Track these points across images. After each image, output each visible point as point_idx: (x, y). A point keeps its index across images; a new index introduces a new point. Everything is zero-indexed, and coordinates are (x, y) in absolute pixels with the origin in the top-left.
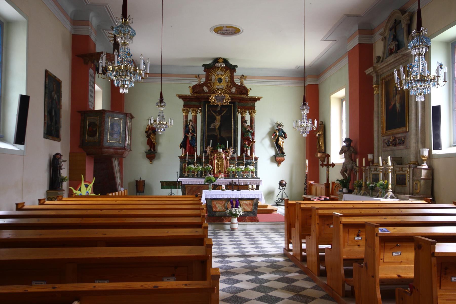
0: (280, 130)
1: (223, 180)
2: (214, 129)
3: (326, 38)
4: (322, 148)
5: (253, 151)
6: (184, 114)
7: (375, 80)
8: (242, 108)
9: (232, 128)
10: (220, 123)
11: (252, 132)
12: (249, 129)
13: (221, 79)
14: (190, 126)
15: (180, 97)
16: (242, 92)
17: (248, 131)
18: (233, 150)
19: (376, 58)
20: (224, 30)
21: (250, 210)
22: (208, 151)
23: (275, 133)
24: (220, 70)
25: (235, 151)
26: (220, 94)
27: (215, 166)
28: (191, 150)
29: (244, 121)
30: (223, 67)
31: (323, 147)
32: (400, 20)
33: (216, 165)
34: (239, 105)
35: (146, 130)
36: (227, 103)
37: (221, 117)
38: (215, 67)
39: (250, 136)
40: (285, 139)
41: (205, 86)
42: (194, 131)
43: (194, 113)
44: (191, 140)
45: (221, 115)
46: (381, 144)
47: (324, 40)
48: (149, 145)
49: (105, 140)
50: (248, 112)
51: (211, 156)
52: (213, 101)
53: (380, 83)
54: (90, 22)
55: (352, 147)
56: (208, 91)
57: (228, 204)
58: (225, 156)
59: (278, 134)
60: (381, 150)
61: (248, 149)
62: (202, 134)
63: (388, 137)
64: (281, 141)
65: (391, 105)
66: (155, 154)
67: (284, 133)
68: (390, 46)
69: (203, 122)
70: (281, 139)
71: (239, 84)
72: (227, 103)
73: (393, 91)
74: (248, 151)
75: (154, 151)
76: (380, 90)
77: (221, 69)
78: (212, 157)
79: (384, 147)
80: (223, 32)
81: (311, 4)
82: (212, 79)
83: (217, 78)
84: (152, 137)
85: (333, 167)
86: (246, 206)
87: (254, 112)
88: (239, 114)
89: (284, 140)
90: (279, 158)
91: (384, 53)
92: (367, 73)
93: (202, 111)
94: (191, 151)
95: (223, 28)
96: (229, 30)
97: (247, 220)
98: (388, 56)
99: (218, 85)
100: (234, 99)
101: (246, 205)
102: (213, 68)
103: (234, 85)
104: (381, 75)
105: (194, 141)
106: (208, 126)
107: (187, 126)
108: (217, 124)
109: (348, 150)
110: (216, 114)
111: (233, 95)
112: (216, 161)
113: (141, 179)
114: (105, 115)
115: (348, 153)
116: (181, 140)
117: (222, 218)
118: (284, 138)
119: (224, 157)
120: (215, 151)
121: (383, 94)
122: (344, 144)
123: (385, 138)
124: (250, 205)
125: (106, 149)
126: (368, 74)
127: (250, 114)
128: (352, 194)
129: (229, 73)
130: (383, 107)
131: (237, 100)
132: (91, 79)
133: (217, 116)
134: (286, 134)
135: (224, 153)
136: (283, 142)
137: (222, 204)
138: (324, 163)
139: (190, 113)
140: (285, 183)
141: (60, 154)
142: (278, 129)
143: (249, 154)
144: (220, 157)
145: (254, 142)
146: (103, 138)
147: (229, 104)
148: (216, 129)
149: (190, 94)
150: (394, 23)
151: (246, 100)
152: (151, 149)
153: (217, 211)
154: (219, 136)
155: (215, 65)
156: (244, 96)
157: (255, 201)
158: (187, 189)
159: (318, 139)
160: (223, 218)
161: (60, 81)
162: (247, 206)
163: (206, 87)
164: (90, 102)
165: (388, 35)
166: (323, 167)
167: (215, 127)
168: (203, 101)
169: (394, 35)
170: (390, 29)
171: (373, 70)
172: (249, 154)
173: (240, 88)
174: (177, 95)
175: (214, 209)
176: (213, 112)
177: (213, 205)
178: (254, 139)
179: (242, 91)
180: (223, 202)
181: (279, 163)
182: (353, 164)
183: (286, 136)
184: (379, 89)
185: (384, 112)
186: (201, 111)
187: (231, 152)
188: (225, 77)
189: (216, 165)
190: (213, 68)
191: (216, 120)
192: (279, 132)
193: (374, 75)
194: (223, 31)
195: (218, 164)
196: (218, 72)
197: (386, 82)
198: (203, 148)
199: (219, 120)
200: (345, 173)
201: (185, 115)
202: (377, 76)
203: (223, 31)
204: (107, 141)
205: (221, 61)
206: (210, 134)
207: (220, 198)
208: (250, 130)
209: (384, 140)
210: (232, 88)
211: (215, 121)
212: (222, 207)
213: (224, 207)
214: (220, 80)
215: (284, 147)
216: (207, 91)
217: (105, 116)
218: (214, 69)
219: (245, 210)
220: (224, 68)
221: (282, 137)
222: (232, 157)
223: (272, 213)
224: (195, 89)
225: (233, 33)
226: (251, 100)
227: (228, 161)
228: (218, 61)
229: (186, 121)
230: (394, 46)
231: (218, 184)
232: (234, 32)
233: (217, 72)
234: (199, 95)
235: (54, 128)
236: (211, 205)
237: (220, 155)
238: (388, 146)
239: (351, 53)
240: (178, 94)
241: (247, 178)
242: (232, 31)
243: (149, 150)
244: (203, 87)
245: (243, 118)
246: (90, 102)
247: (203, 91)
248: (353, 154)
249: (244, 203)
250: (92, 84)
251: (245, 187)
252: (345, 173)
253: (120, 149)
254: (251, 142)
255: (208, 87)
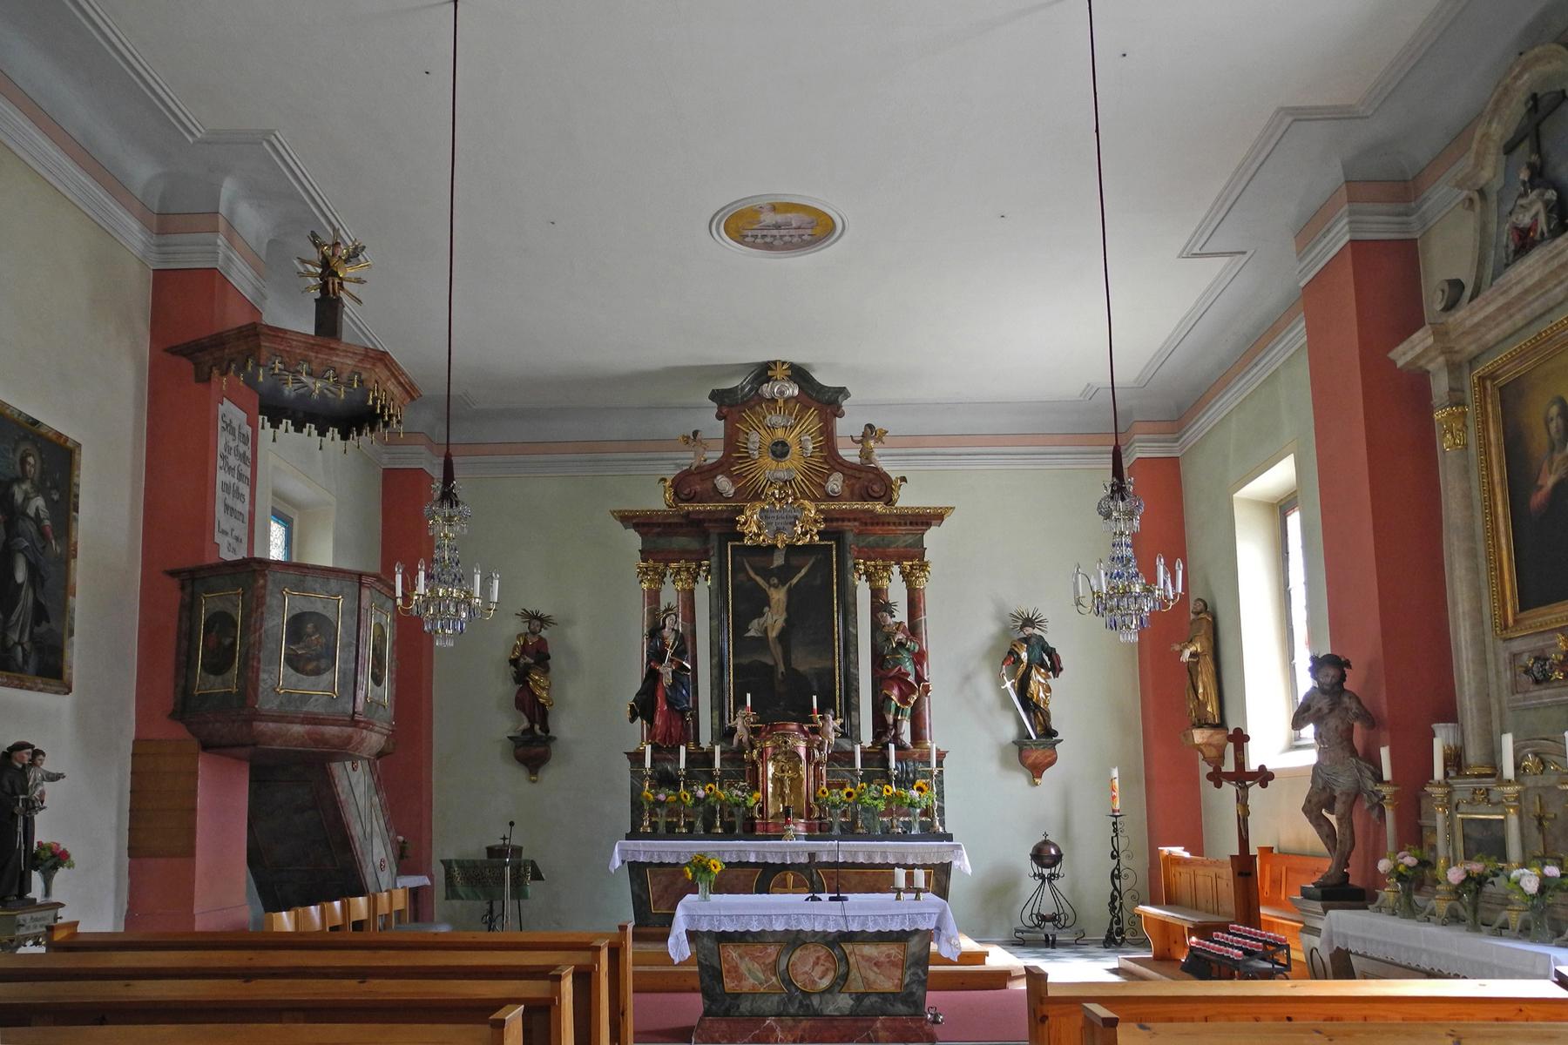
0: (1033, 640)
1: (801, 845)
2: (762, 642)
3: (1199, 245)
4: (1209, 709)
5: (925, 724)
6: (645, 586)
7: (1440, 385)
8: (873, 555)
9: (836, 636)
10: (784, 616)
11: (917, 648)
12: (900, 636)
13: (784, 444)
14: (666, 630)
15: (629, 519)
16: (870, 490)
17: (901, 644)
18: (839, 721)
19: (1443, 291)
20: (768, 227)
21: (893, 989)
22: (738, 727)
23: (1013, 654)
24: (780, 408)
25: (849, 732)
26: (780, 500)
27: (770, 790)
28: (674, 723)
29: (880, 605)
30: (792, 397)
31: (1214, 704)
32: (1558, 88)
33: (770, 785)
34: (861, 544)
35: (513, 653)
36: (808, 536)
37: (790, 592)
38: (762, 399)
39: (909, 667)
40: (1056, 675)
41: (721, 473)
42: (685, 646)
43: (681, 580)
44: (673, 687)
45: (787, 585)
46: (1498, 673)
47: (1195, 255)
48: (523, 710)
49: (262, 686)
50: (896, 569)
51: (753, 747)
52: (755, 529)
53: (1470, 396)
54: (221, 219)
55: (1353, 696)
56: (735, 493)
57: (793, 958)
58: (808, 750)
59: (1024, 656)
60: (1500, 702)
61: (902, 720)
62: (715, 660)
63: (1537, 643)
64: (1039, 682)
65: (1541, 487)
66: (549, 746)
67: (1051, 653)
68: (1513, 219)
69: (716, 614)
70: (1039, 678)
71: (857, 460)
72: (808, 536)
73: (1547, 422)
74: (901, 726)
75: (544, 734)
76: (1472, 429)
77: (782, 405)
78: (755, 752)
79: (1515, 688)
80: (764, 236)
81: (1124, 55)
82: (750, 446)
83: (768, 441)
84: (535, 681)
85: (1264, 785)
86: (875, 969)
87: (923, 566)
88: (860, 579)
89: (1052, 682)
90: (1036, 755)
91: (1481, 262)
92: (1400, 364)
93: (713, 571)
94: (673, 730)
95: (762, 217)
96: (788, 225)
97: (881, 1034)
98: (1507, 265)
99: (771, 469)
100: (837, 520)
101: (875, 964)
102: (752, 403)
103: (837, 467)
104: (1470, 362)
105: (684, 692)
106: (740, 627)
107: (655, 632)
108: (774, 619)
109: (1331, 710)
110: (768, 583)
111: (834, 506)
112: (771, 769)
113: (507, 842)
114: (266, 581)
115: (1333, 722)
116: (636, 685)
117: (768, 1022)
118: (1050, 674)
119: (802, 753)
120: (766, 727)
121: (1490, 444)
122: (1343, 659)
123: (1516, 646)
124: (893, 964)
125: (271, 725)
126: (1407, 364)
127: (907, 576)
128: (1367, 908)
129: (817, 419)
130: (1495, 504)
131: (849, 524)
132: (232, 444)
133: (772, 589)
134: (1057, 656)
135: (802, 736)
136: (1048, 689)
137: (767, 962)
138: (1224, 769)
139: (668, 579)
140: (1058, 851)
141: (32, 747)
142: (1024, 638)
143: (906, 738)
144: (786, 754)
145: (927, 690)
146: (257, 676)
147: (817, 538)
148: (770, 639)
149: (665, 507)
150: (1529, 110)
151: (889, 524)
152: (532, 727)
153: (745, 990)
154: (781, 668)
155: (760, 392)
156: (879, 507)
157: (914, 945)
158: (653, 885)
159: (1191, 670)
160: (773, 1024)
161: (69, 444)
162: (878, 971)
163: (725, 479)
164: (224, 533)
165: (1495, 176)
166: (1218, 785)
167: (766, 631)
168: (717, 531)
169: (1531, 166)
170: (1505, 146)
171: (1430, 340)
172: (906, 738)
173: (860, 478)
174: (613, 513)
175: (729, 985)
176: (757, 574)
177: (725, 967)
178: (926, 678)
179: (867, 487)
180: (769, 951)
181: (1036, 771)
182: (1359, 771)
183: (1057, 663)
184: (1465, 425)
185: (1502, 528)
186: (709, 572)
187: (830, 729)
188: (802, 438)
189: (770, 785)
190: (752, 403)
191: (770, 607)
192: (1028, 651)
193: (1437, 367)
194: (765, 232)
195: (778, 781)
196: (774, 419)
197: (1500, 389)
198: (722, 717)
199: (783, 605)
200: (1323, 811)
201: (649, 589)
202: (1454, 368)
203: (765, 232)
204: (274, 689)
205: (779, 373)
206: (745, 661)
207: (754, 929)
208: (907, 639)
209: (1515, 657)
210: (828, 478)
211: (766, 609)
212: (764, 972)
213: (775, 975)
214: (779, 447)
215: (1053, 708)
216: (733, 491)
217: (264, 587)
218: (757, 408)
219: (869, 988)
220: (794, 401)
221: (1042, 670)
222: (839, 750)
223: (1005, 987)
224: (685, 485)
225: (805, 237)
226: (905, 524)
227: (824, 770)
228: (770, 373)
229: (654, 613)
230: (1537, 214)
231: (779, 862)
232: (809, 232)
233: (769, 417)
234: (699, 507)
235: (26, 638)
236: (716, 964)
237: (786, 742)
238: (1537, 682)
239: (1314, 295)
240: (617, 508)
241: (905, 837)
242: (799, 228)
243: (524, 732)
244: (715, 477)
245: (877, 593)
246: (224, 533)
247: (717, 495)
248: (1357, 725)
249: (863, 957)
250: (238, 463)
251: (875, 878)
252: (1323, 811)
253: (335, 723)
254: (912, 690)
255: (735, 478)
